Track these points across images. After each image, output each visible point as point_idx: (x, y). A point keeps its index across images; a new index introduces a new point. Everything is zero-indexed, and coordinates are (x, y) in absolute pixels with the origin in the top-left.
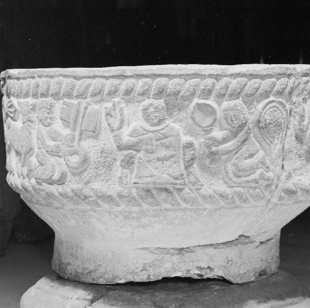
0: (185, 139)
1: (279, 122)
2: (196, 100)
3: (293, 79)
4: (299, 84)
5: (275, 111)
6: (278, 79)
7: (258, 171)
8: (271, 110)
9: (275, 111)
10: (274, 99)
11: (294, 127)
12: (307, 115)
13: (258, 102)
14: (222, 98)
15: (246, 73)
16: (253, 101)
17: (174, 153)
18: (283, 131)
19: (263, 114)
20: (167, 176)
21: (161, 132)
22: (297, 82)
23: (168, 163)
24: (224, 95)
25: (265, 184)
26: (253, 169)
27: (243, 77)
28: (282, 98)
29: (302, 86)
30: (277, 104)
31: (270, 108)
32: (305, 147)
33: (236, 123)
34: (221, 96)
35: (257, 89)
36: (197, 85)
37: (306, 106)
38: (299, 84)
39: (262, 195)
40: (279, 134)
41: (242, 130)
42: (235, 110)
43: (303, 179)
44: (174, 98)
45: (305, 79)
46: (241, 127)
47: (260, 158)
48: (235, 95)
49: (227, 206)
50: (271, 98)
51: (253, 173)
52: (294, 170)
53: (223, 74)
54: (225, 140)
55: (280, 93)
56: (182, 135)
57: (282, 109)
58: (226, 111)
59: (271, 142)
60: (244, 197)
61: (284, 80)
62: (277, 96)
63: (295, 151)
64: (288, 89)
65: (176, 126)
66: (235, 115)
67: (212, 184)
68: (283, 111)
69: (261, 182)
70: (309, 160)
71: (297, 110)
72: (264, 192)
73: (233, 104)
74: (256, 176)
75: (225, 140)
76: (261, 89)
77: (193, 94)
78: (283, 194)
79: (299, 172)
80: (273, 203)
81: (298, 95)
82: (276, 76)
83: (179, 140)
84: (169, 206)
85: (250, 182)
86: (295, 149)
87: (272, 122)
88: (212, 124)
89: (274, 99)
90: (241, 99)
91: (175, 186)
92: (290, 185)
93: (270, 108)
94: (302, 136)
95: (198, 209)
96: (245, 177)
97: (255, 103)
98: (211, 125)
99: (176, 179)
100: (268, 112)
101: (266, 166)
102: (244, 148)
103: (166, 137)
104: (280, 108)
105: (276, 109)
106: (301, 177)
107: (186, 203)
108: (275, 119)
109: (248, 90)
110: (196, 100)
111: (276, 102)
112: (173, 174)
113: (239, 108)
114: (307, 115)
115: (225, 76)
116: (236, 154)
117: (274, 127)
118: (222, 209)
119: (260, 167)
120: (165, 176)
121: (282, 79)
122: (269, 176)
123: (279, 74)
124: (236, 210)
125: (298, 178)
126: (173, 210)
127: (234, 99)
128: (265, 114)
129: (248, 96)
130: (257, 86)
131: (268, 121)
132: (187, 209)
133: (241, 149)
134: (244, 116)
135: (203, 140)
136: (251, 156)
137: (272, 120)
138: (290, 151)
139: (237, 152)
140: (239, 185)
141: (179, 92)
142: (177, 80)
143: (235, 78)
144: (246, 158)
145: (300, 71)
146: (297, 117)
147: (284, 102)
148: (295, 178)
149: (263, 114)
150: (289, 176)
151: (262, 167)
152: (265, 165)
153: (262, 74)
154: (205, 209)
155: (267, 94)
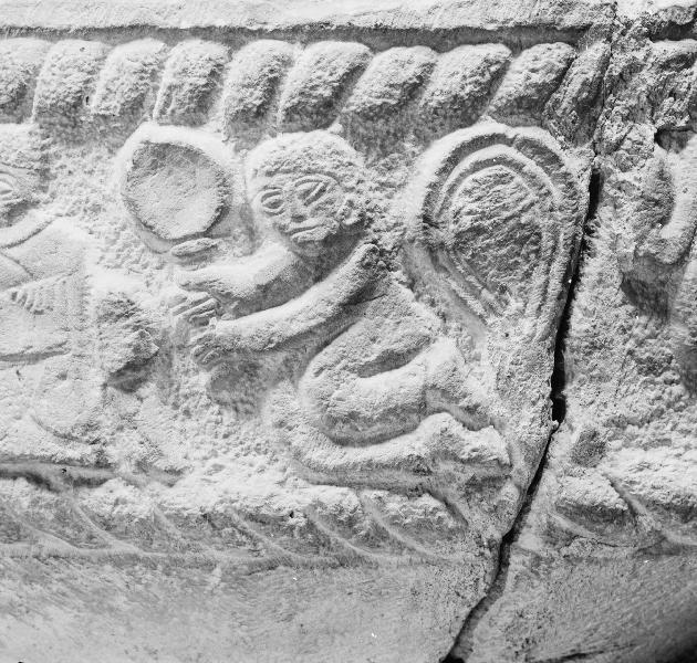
0: (106, 283)
1: (523, 226)
2: (151, 131)
3: (594, 51)
4: (634, 68)
5: (501, 179)
6: (516, 49)
7: (431, 426)
8: (481, 174)
9: (501, 179)
10: (500, 128)
11: (613, 246)
12: (684, 199)
13: (424, 141)
14: (253, 124)
15: (356, 24)
16: (399, 135)
17: (60, 337)
18: (550, 261)
19: (444, 189)
20: (33, 427)
21: (14, 252)
22: (619, 64)
23: (35, 372)
24: (261, 112)
25: (464, 478)
26: (405, 416)
27: (345, 39)
28: (542, 125)
29: (648, 78)
30: (512, 153)
31: (478, 166)
32: (680, 333)
33: (317, 227)
34: (251, 120)
35: (272, 86)
36: (151, 73)
37: (680, 165)
38: (634, 68)
39: (451, 523)
40: (528, 275)
41: (344, 255)
42: (308, 172)
43: (663, 468)
44: (65, 120)
45: (667, 49)
46: (338, 243)
47: (431, 372)
48: (318, 111)
49: (297, 557)
50: (486, 126)
51: (404, 432)
52: (619, 424)
53: (254, 28)
54: (270, 294)
55: (533, 106)
56: (90, 267)
57: (539, 171)
58: (270, 174)
59: (490, 308)
60: (365, 525)
61: (551, 54)
62: (514, 119)
63: (620, 347)
64: (573, 87)
65: (72, 230)
66: (308, 192)
67: (218, 468)
68: (547, 179)
69: (445, 467)
70: (693, 385)
71: (627, 176)
72: (462, 507)
73: (299, 147)
74: (413, 445)
75: (270, 294)
76: (431, 88)
77: (134, 109)
78: (563, 522)
79: (646, 433)
80: (525, 552)
81: (631, 116)
82: (505, 35)
83: (83, 292)
84: (63, 547)
85: (386, 466)
86: (619, 338)
87: (486, 223)
88: (209, 229)
89: (500, 128)
90: (336, 127)
91: (68, 468)
92: (592, 487)
93: (478, 166)
94: (663, 283)
95: (176, 562)
96: (363, 443)
97: (408, 145)
98: (207, 233)
99: (67, 438)
100: (467, 183)
101: (464, 403)
102: (357, 332)
103: (32, 275)
104: (531, 165)
105: (506, 170)
106: (655, 456)
107: (120, 536)
108: (506, 214)
109: (365, 92)
110: (151, 131)
111: (510, 142)
112: (55, 424)
113: (327, 164)
114: (684, 199)
115: (260, 34)
116: (319, 349)
117: (500, 244)
118: (281, 568)
119: (436, 405)
120: (26, 426)
121: (538, 49)
122: (477, 445)
123: (519, 27)
124: (347, 576)
125: (638, 456)
126: (83, 560)
127: (305, 129)
128: (452, 190)
129: (369, 114)
130: (409, 74)
131: (467, 221)
132: (134, 559)
133: (346, 329)
134: (350, 196)
135: (174, 290)
136: (391, 361)
137: (483, 216)
138: (594, 347)
139: (327, 344)
140: (338, 477)
141: (79, 101)
142: (70, 49)
143: (305, 43)
144: (365, 371)
145: (632, 17)
146: (629, 207)
147: (553, 144)
148: (623, 461)
149: (444, 189)
150: (591, 450)
151: (445, 405)
152: (457, 400)
153: (436, 26)
154: (209, 566)
155: (464, 110)
